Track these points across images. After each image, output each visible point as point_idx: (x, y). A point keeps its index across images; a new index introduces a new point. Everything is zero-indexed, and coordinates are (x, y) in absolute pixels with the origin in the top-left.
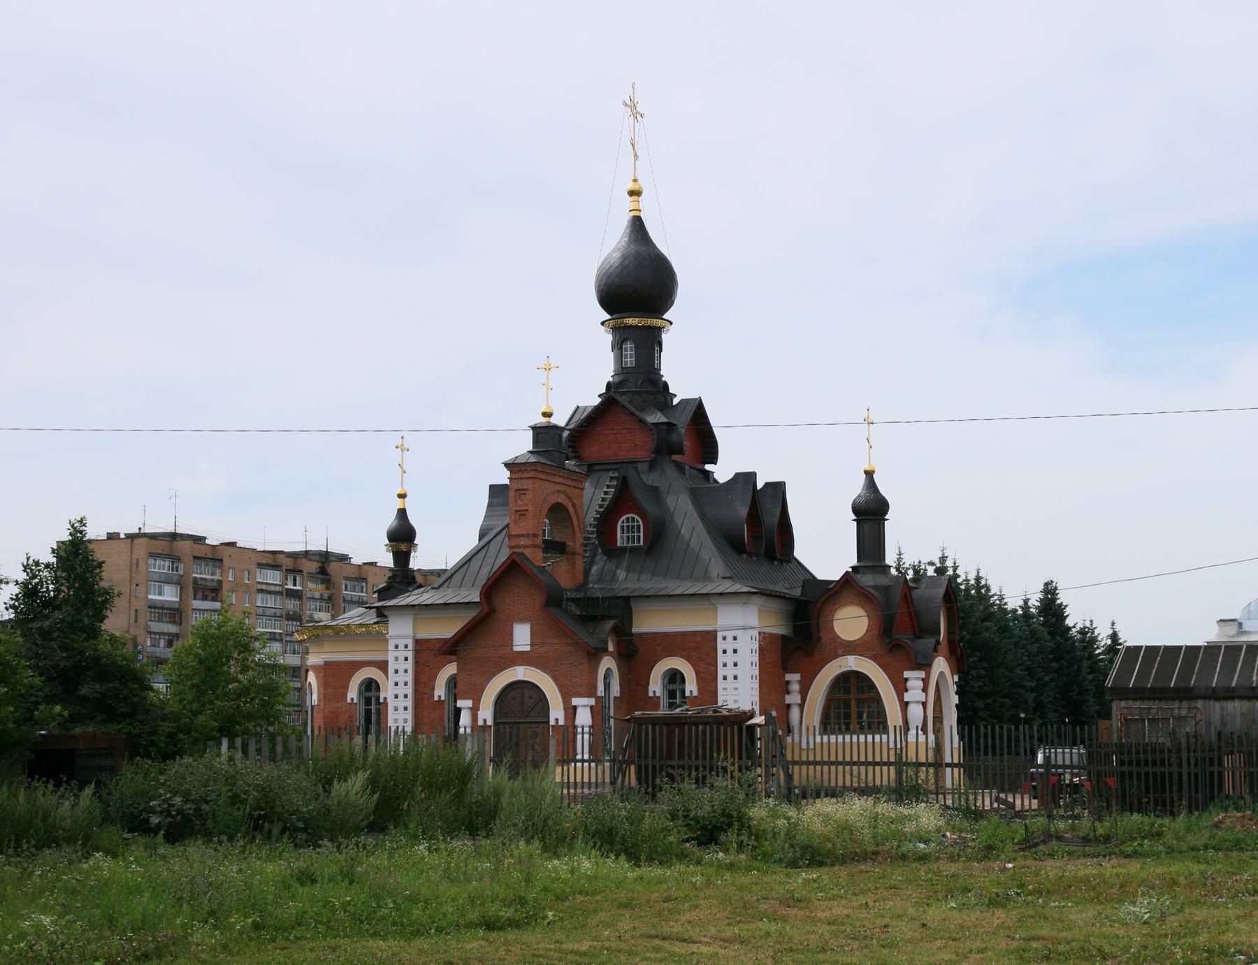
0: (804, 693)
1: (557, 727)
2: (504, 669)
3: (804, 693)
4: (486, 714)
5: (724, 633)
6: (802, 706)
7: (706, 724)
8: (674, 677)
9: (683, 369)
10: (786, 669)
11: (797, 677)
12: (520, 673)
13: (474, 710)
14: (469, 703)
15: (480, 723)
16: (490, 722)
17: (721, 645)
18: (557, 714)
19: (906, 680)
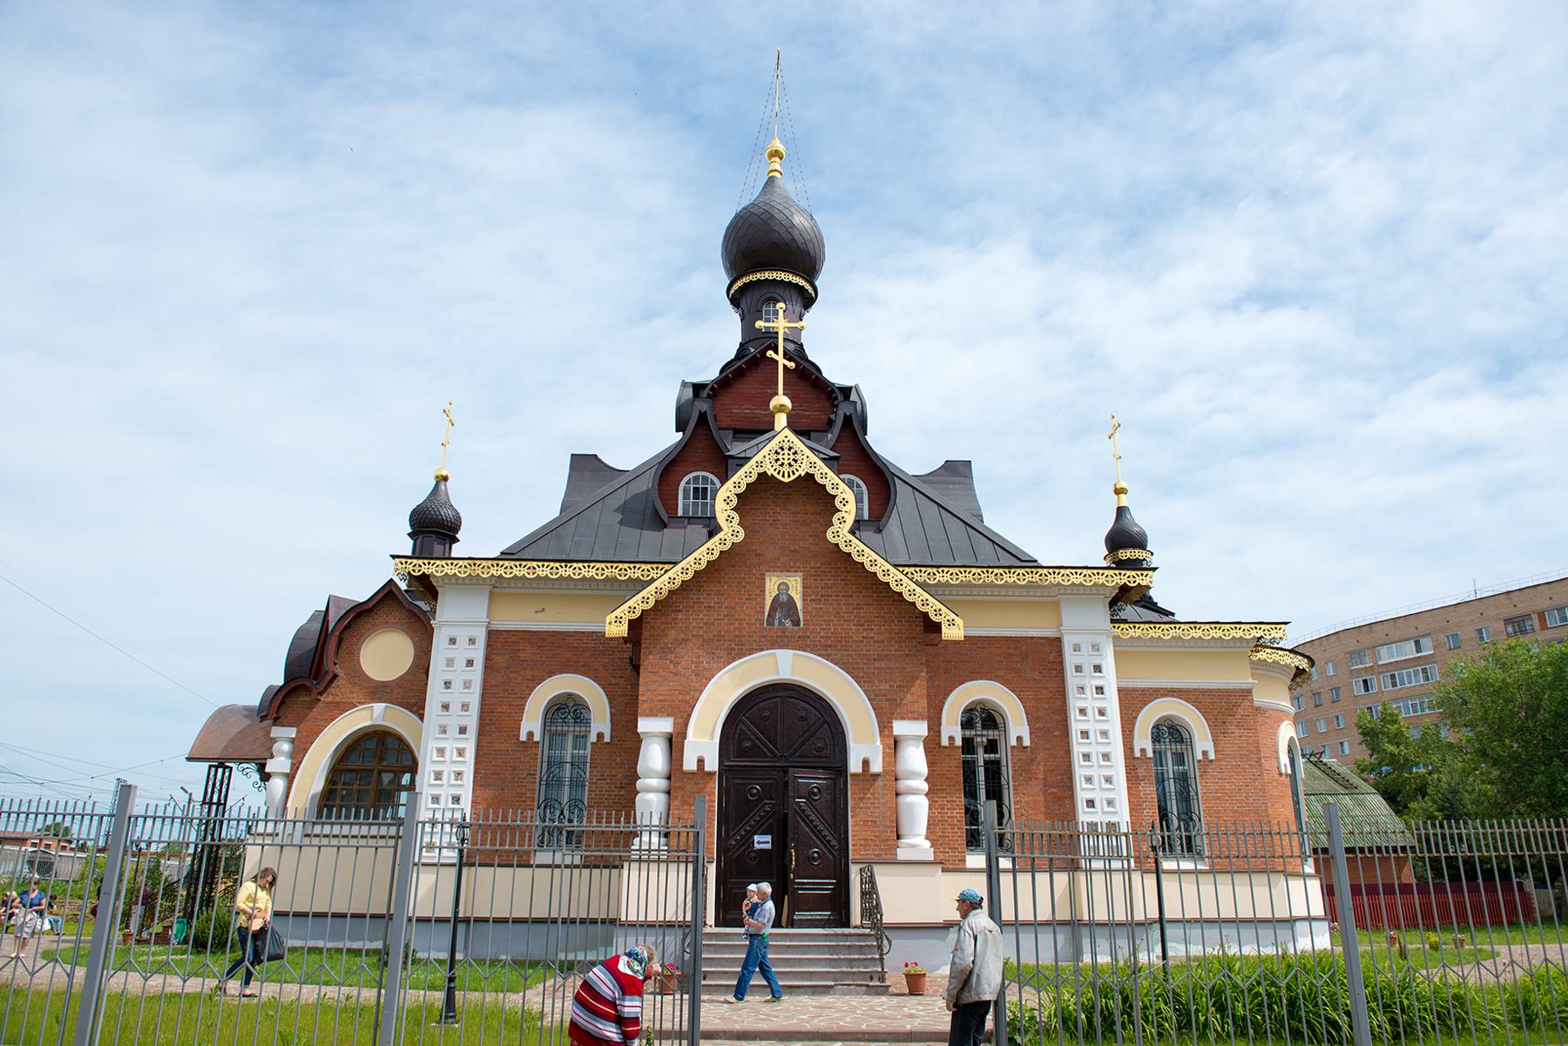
0: (297, 756)
1: (854, 775)
2: (751, 651)
3: (297, 756)
4: (704, 745)
5: (453, 632)
6: (290, 778)
7: (1412, 697)
8: (566, 710)
9: (836, 336)
10: (277, 721)
11: (292, 732)
12: (786, 665)
13: (674, 744)
14: (666, 725)
15: (690, 764)
16: (712, 765)
17: (1070, 659)
18: (863, 749)
19: (274, 740)
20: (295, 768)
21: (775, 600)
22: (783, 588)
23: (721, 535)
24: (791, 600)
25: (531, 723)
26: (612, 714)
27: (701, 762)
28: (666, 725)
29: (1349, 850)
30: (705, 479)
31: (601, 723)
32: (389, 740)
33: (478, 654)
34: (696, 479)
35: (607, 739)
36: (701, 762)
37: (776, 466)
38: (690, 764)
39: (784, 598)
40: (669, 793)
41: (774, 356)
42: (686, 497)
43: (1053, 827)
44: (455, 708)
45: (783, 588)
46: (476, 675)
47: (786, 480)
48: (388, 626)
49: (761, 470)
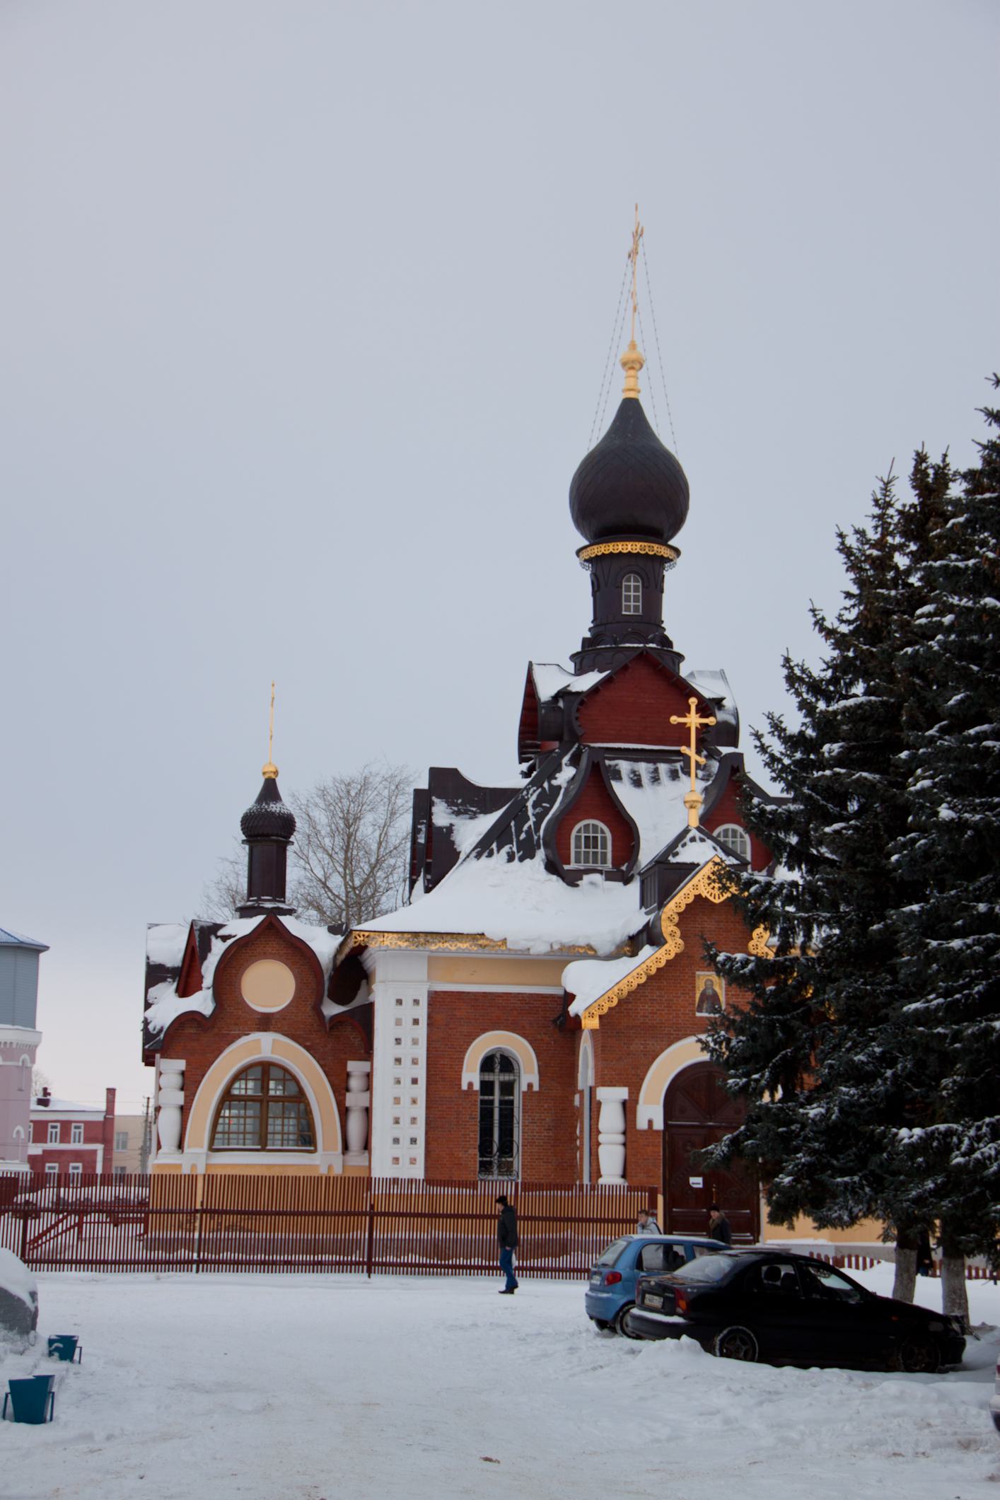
11: (181, 1064)
13: (629, 1108)
14: (623, 1093)
16: (659, 1125)
20: (189, 1099)
21: (703, 994)
22: (709, 984)
23: (666, 947)
24: (715, 996)
25: (471, 1076)
26: (539, 1066)
27: (650, 1122)
28: (623, 1093)
29: (212, 1149)
30: (595, 827)
31: (529, 1075)
32: (274, 1072)
33: (422, 1012)
34: (587, 826)
35: (536, 1088)
36: (650, 1122)
37: (709, 889)
38: (642, 1124)
39: (710, 992)
40: (624, 1145)
41: (698, 758)
42: (578, 846)
43: (982, 1154)
44: (406, 1062)
45: (709, 984)
46: (422, 1031)
47: (717, 901)
48: (265, 956)
49: (697, 893)
